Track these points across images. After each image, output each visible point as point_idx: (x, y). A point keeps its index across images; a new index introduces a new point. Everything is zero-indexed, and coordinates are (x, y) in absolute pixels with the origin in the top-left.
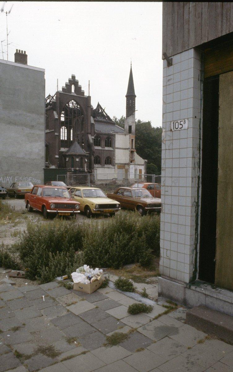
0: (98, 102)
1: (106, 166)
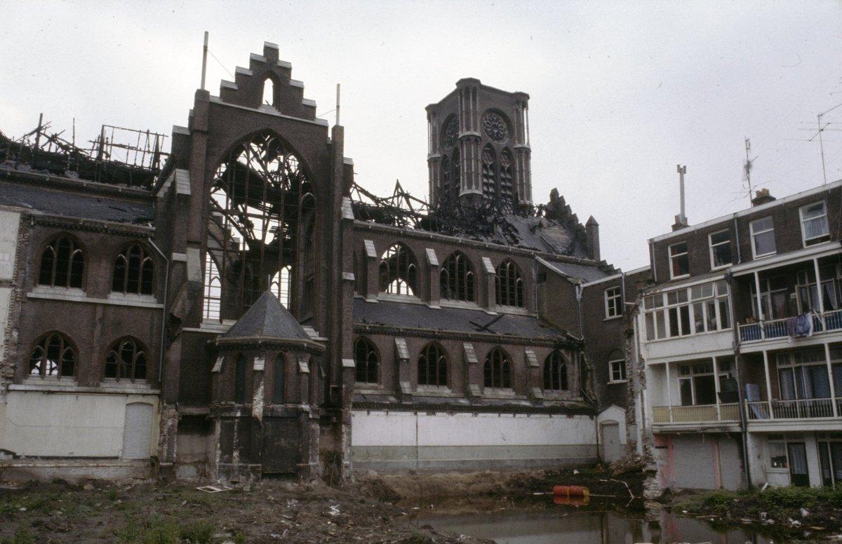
0: (398, 180)
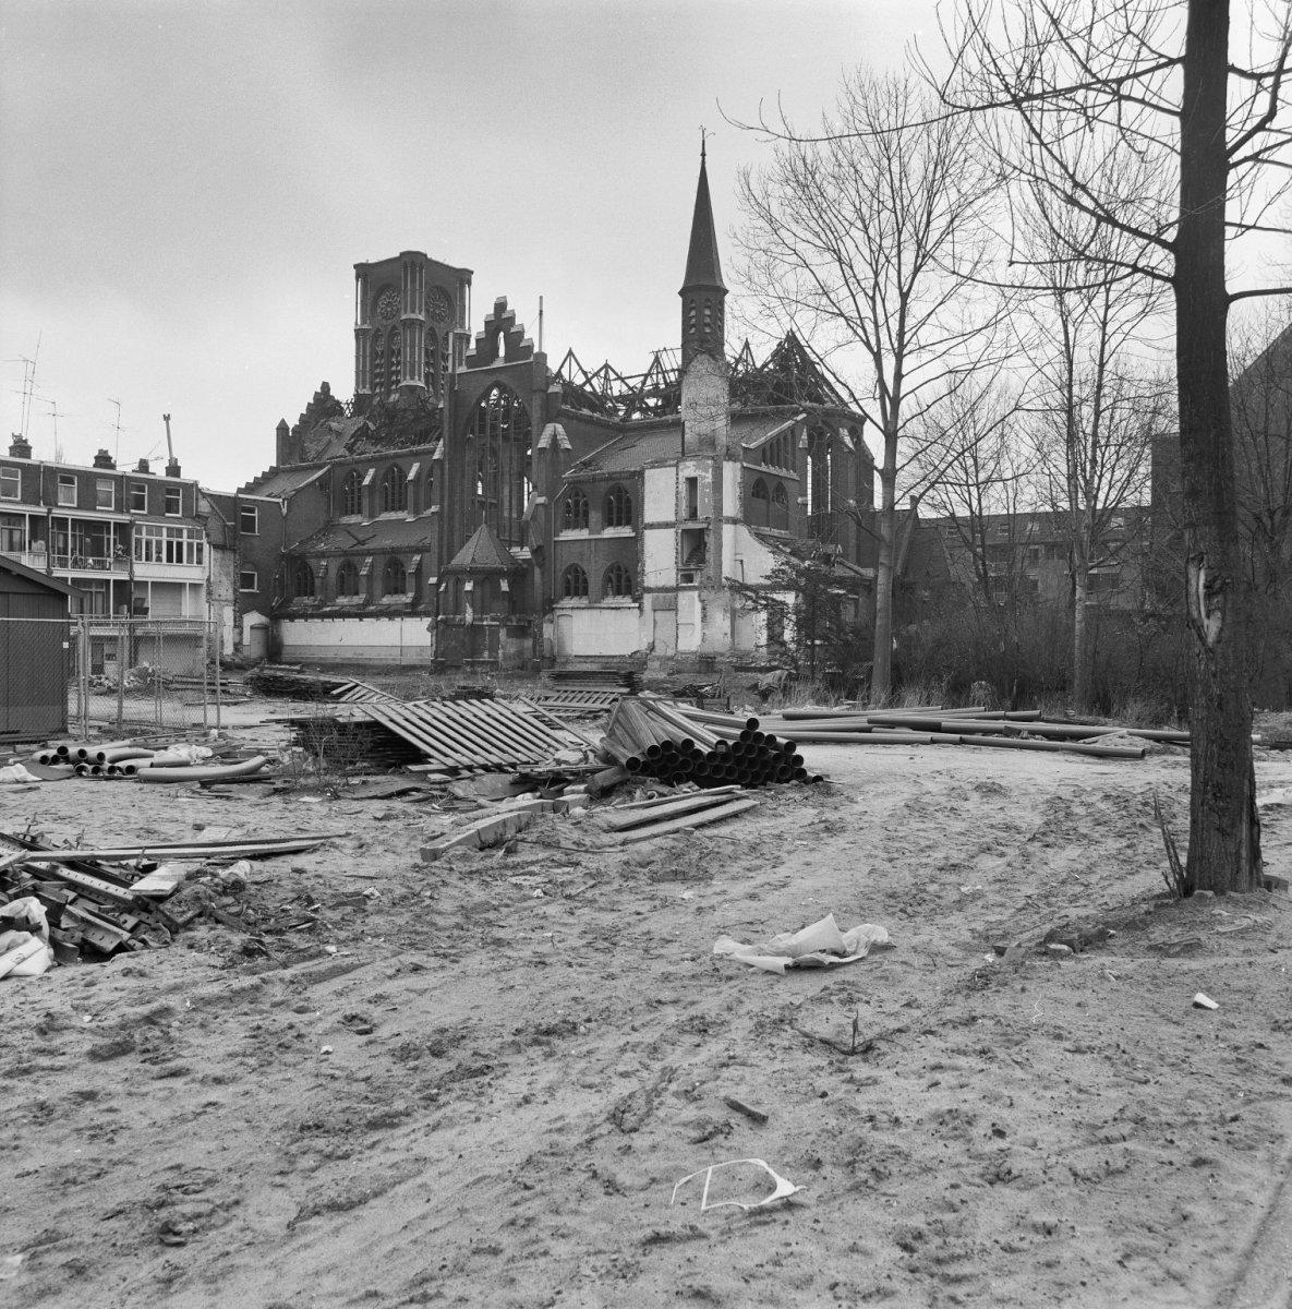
1: (610, 601)
